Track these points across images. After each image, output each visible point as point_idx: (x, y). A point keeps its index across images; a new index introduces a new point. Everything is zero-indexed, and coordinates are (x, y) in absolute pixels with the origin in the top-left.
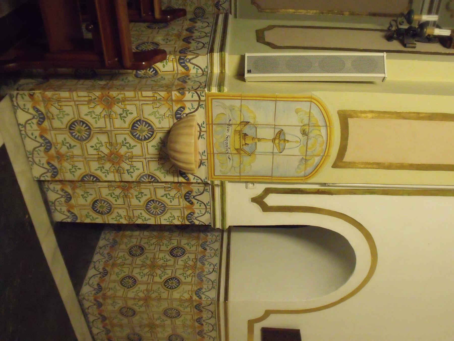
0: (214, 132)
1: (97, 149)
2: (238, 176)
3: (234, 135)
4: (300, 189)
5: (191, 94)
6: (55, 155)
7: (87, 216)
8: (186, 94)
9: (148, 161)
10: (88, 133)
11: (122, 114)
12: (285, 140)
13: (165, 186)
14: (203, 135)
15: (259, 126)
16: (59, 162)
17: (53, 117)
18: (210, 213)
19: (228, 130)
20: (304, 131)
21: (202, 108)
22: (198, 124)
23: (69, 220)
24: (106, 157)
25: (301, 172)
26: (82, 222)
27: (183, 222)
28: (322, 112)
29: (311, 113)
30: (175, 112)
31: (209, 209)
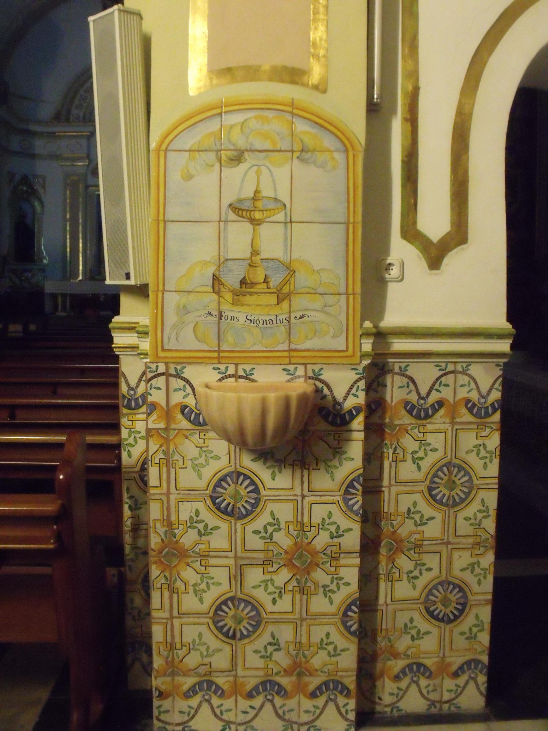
0: (237, 349)
1: (280, 592)
2: (348, 299)
3: (245, 307)
4: (403, 161)
5: (153, 392)
6: (294, 678)
7: (472, 637)
8: (153, 402)
9: (309, 491)
10: (242, 605)
11: (199, 531)
12: (255, 199)
13: (391, 459)
14: (245, 371)
15: (222, 253)
16: (311, 675)
17: (206, 665)
18: (469, 364)
19: (233, 318)
20: (232, 160)
21: (407, 368)
22: (220, 380)
23: (482, 679)
24: (298, 577)
25: (333, 158)
26: (487, 652)
27: (494, 427)
28: (189, 127)
29: (193, 148)
30: (191, 425)
31: (455, 366)
